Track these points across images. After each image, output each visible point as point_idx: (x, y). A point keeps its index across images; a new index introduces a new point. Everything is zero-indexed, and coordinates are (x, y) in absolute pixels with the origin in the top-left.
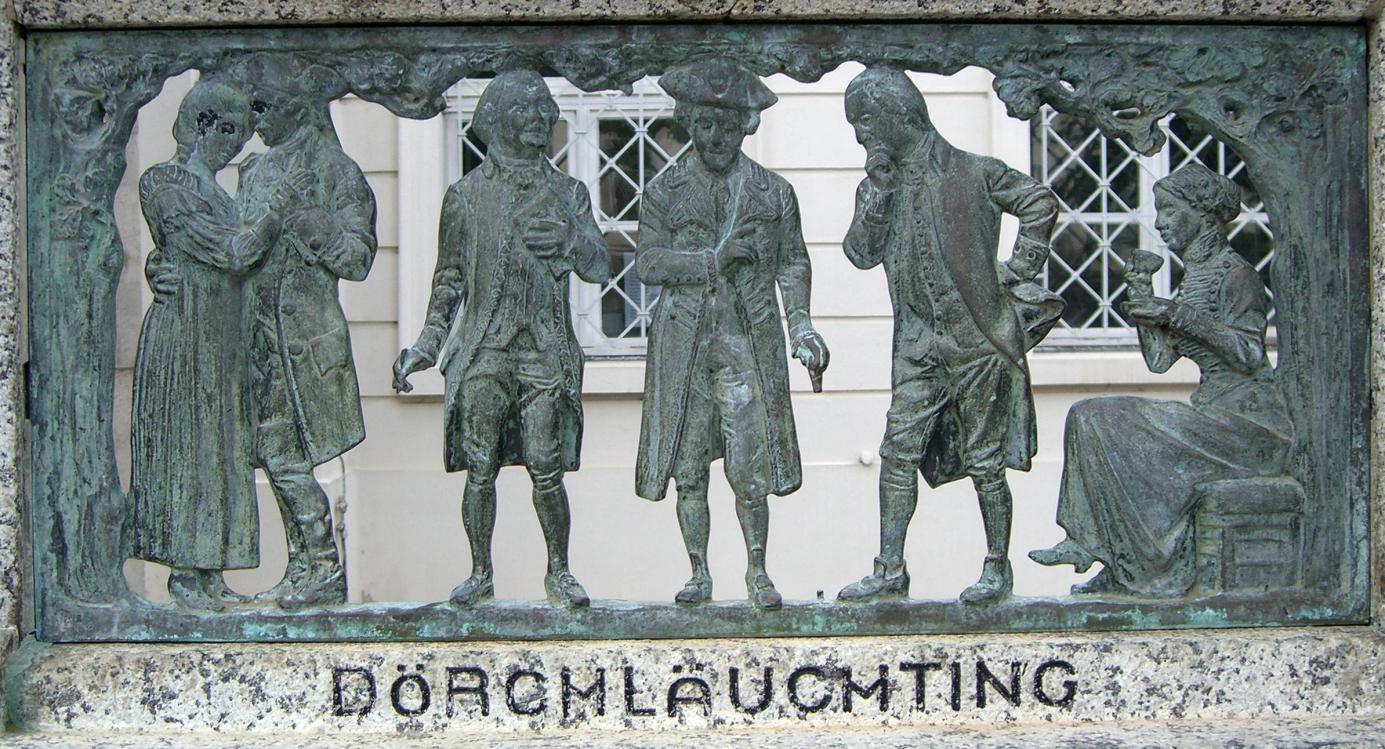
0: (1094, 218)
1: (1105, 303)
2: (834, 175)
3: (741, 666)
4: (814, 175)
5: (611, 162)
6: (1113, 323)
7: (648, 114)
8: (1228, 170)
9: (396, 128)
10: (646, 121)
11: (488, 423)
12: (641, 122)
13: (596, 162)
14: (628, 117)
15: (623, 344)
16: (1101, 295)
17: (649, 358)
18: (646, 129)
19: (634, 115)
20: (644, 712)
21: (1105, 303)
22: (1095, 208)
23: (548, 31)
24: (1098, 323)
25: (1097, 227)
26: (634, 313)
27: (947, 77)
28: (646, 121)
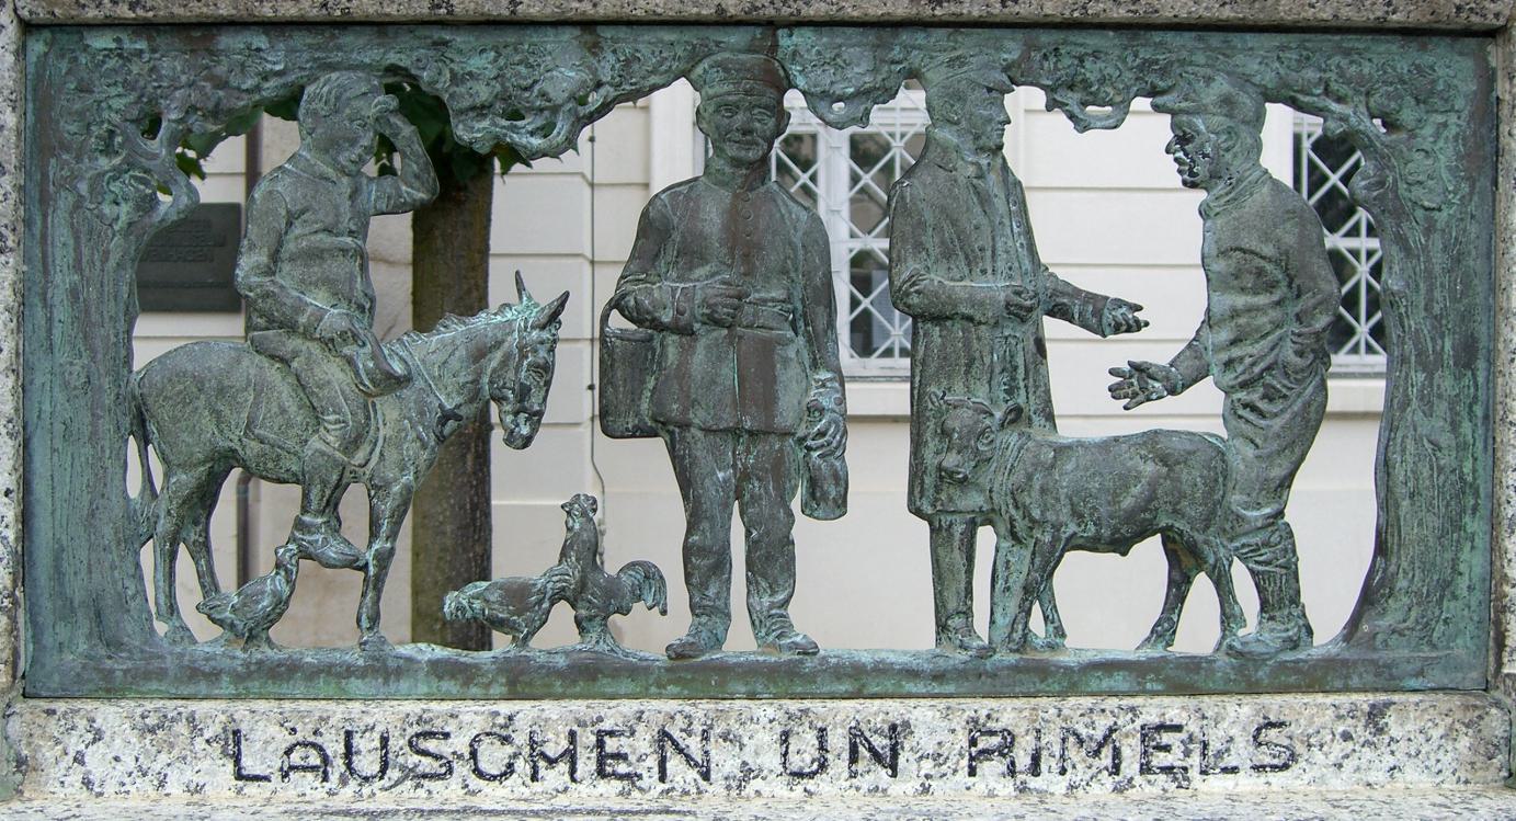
0: (1353, 243)
1: (1363, 330)
2: (1092, 195)
3: (575, 728)
4: (1075, 195)
5: (867, 179)
6: (1370, 350)
7: (904, 129)
8: (1310, 194)
9: (1135, 113)
10: (903, 136)
11: (1034, 457)
12: (898, 136)
13: (821, 178)
14: (884, 131)
15: (874, 364)
16: (892, 324)
17: (1387, 375)
18: (902, 144)
19: (891, 129)
20: (257, 778)
21: (1363, 330)
22: (1354, 232)
23: (941, 32)
24: (1355, 350)
25: (1355, 253)
26: (887, 335)
27: (690, 117)
28: (903, 136)
